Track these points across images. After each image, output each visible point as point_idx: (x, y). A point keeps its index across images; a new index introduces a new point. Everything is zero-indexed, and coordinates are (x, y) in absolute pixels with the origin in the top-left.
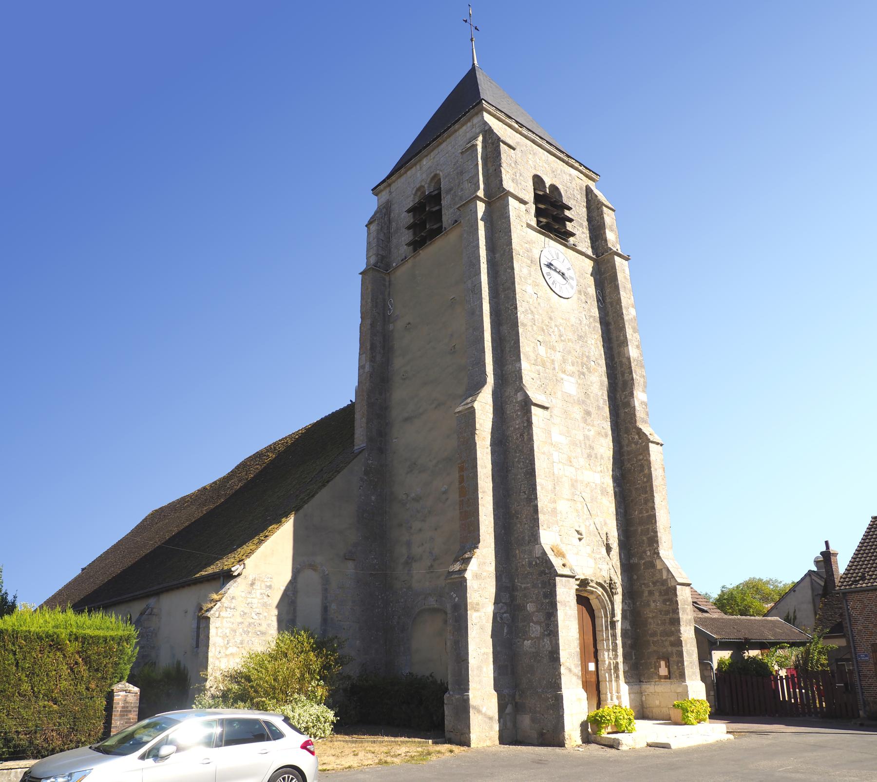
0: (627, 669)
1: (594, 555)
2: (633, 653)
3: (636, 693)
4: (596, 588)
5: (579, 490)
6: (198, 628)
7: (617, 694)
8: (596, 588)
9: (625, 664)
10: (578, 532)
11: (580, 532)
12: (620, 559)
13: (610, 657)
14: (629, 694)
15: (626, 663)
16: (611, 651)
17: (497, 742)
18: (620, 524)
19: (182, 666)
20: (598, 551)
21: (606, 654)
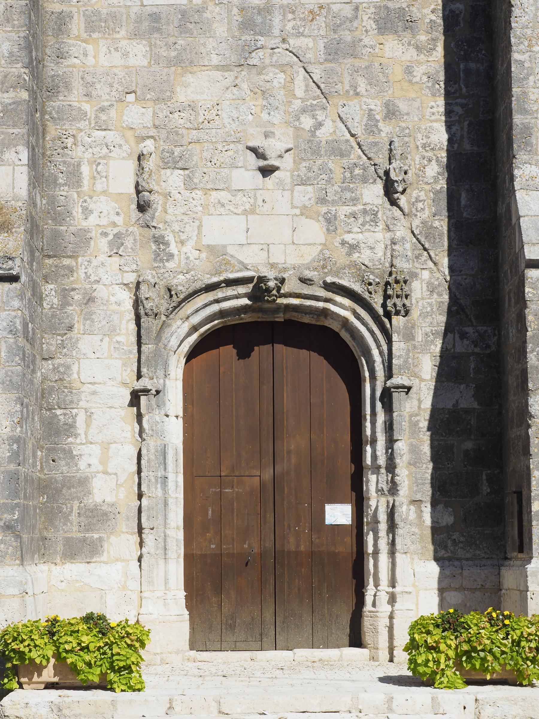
0: (448, 519)
1: (324, 209)
2: (484, 477)
3: (473, 590)
4: (327, 300)
5: (277, 32)
6: (192, 315)
7: (391, 589)
8: (327, 300)
9: (440, 507)
10: (254, 150)
11: (261, 151)
12: (450, 209)
13: (380, 485)
14: (441, 590)
15: (446, 506)
16: (383, 471)
17: (188, 647)
18: (463, 106)
19: (237, 358)
20: (348, 195)
21: (373, 478)
